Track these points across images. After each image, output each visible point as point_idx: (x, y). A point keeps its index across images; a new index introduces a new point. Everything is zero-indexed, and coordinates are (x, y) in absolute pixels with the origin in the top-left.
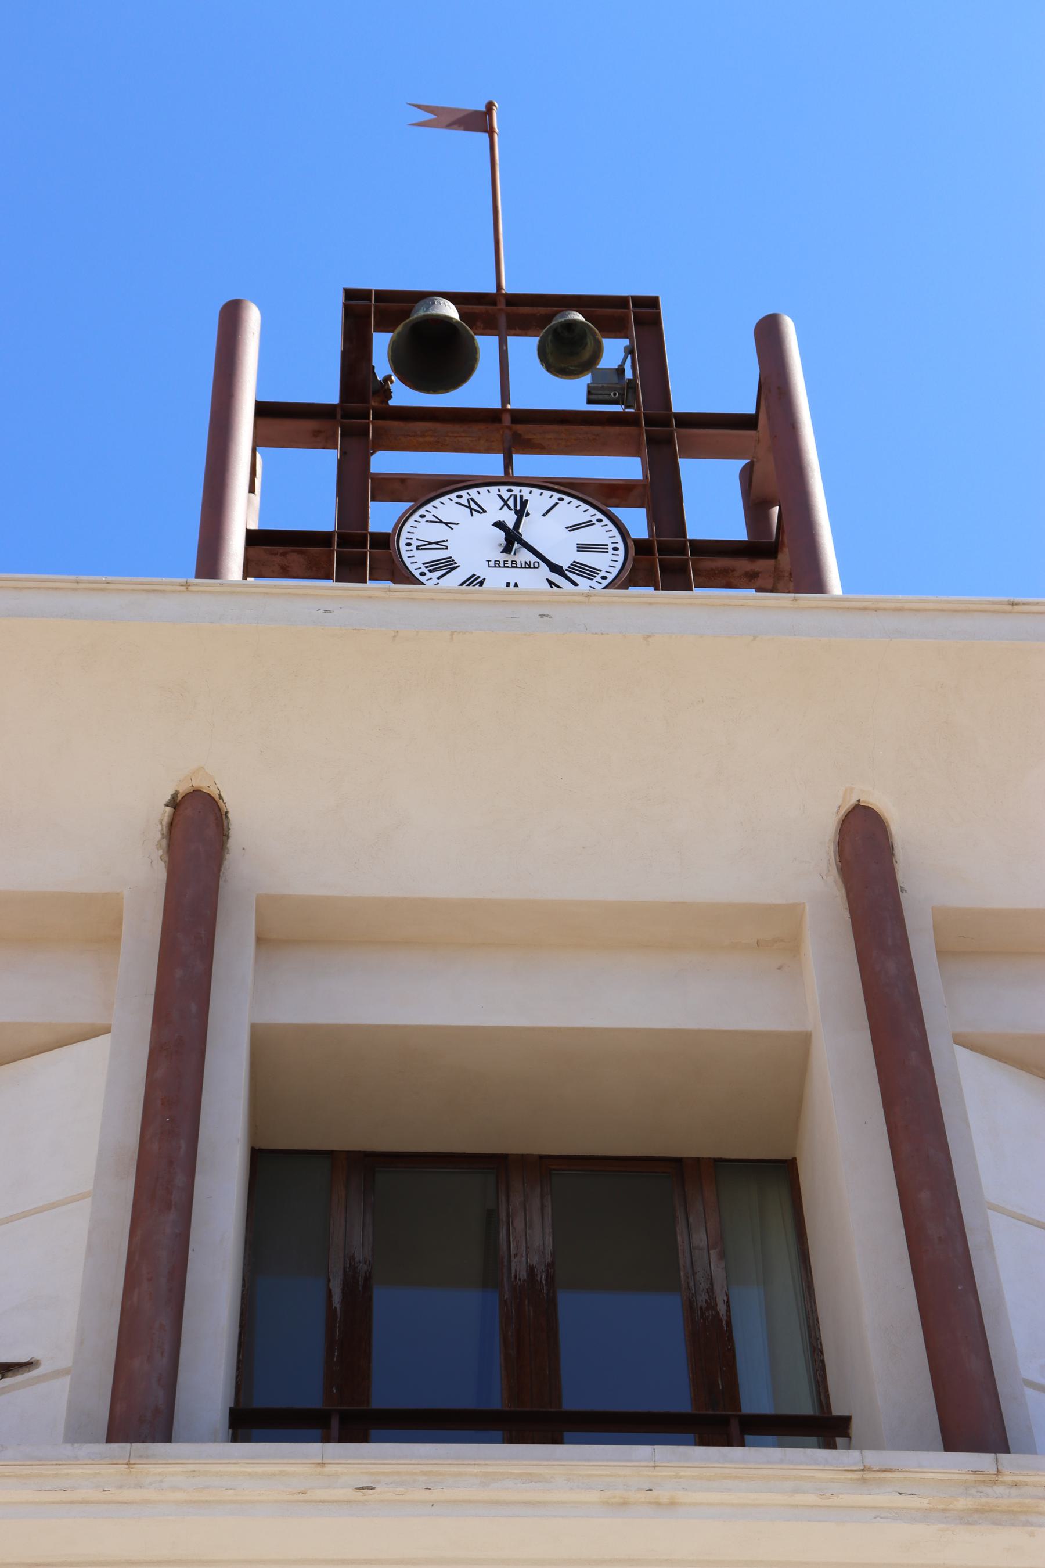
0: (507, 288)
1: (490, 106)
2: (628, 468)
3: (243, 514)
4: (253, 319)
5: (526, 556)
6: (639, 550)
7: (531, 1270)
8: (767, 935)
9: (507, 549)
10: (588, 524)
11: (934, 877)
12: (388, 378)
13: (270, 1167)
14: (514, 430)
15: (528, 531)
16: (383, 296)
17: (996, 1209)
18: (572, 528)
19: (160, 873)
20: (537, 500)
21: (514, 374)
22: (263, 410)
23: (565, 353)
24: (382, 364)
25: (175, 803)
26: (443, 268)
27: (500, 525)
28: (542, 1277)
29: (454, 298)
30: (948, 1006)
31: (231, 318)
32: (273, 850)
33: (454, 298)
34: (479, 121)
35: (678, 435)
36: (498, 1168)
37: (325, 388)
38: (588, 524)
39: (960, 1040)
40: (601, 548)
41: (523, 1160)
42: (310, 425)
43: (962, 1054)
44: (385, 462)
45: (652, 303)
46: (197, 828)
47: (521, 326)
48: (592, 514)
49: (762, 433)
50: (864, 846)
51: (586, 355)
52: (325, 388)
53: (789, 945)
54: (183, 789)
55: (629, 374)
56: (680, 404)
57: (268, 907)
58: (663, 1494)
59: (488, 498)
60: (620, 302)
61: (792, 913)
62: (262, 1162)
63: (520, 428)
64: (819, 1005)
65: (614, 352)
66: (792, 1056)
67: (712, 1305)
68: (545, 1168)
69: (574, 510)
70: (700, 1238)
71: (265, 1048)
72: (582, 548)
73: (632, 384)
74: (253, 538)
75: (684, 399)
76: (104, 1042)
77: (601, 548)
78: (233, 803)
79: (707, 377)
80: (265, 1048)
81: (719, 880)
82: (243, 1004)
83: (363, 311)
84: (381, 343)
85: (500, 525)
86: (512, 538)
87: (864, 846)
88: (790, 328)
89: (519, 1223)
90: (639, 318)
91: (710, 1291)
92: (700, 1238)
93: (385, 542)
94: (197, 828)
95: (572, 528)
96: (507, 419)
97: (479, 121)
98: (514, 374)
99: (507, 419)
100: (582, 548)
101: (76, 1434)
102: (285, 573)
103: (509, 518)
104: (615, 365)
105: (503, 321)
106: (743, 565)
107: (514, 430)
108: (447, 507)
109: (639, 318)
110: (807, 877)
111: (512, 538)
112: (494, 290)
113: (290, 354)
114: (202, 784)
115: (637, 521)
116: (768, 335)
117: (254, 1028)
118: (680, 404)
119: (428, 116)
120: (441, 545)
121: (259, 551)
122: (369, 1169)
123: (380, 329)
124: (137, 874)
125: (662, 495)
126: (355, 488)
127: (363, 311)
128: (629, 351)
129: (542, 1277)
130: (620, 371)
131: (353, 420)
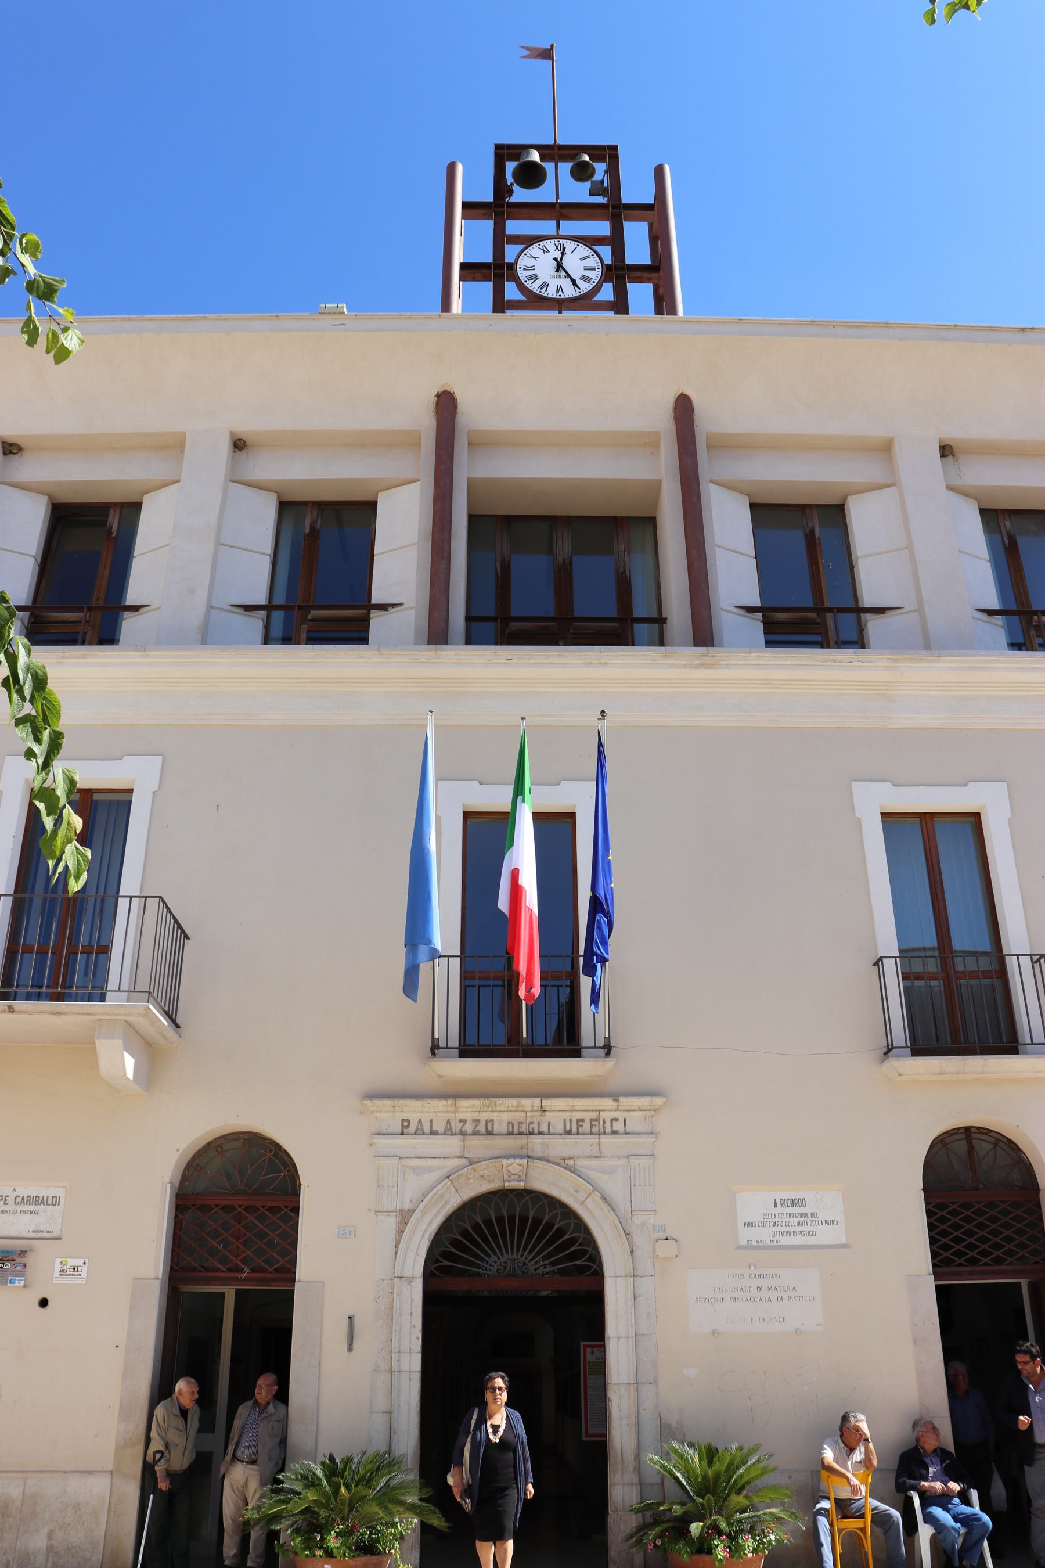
0: (560, 142)
1: (552, 46)
2: (602, 228)
3: (458, 257)
4: (460, 169)
5: (563, 273)
6: (607, 269)
7: (564, 560)
8: (648, 442)
9: (557, 271)
10: (588, 257)
11: (708, 421)
12: (512, 184)
13: (474, 520)
14: (560, 211)
15: (566, 263)
16: (510, 147)
17: (719, 547)
18: (582, 259)
19: (434, 422)
20: (569, 245)
21: (563, 185)
22: (466, 205)
23: (581, 172)
24: (509, 178)
25: (438, 396)
26: (531, 131)
27: (555, 259)
28: (568, 562)
29: (537, 147)
30: (707, 467)
31: (451, 169)
32: (475, 412)
33: (537, 147)
34: (547, 54)
35: (624, 212)
36: (553, 522)
37: (487, 195)
38: (588, 257)
39: (712, 482)
40: (592, 268)
41: (561, 517)
42: (482, 211)
43: (712, 486)
44: (513, 227)
45: (614, 148)
46: (446, 405)
47: (565, 158)
48: (589, 252)
49: (654, 211)
50: (683, 408)
51: (589, 172)
52: (487, 195)
53: (656, 445)
54: (441, 391)
55: (606, 185)
56: (625, 199)
57: (471, 433)
58: (603, 661)
59: (550, 244)
60: (602, 148)
61: (657, 434)
62: (472, 518)
63: (563, 211)
64: (662, 469)
65: (600, 169)
66: (654, 489)
67: (625, 572)
68: (569, 521)
69: (583, 250)
70: (622, 547)
71: (472, 484)
72: (586, 268)
73: (606, 189)
74: (463, 266)
75: (627, 197)
76: (417, 485)
77: (592, 268)
78: (458, 395)
79: (635, 189)
80: (472, 484)
81: (632, 423)
82: (466, 469)
83: (503, 153)
84: (510, 167)
85: (555, 259)
86: (559, 266)
87: (683, 408)
88: (667, 169)
89: (560, 542)
90: (609, 154)
91: (624, 567)
92: (622, 547)
93: (512, 267)
94: (446, 405)
95: (582, 259)
96: (558, 207)
97: (547, 54)
98: (563, 185)
99: (558, 207)
100: (586, 268)
101: (416, 643)
102: (474, 279)
103: (558, 255)
104: (600, 179)
105: (557, 157)
106: (647, 275)
107: (560, 211)
108: (535, 250)
109: (609, 154)
110: (663, 422)
111: (559, 266)
112: (552, 143)
113: (474, 182)
114: (448, 389)
115: (606, 252)
116: (659, 172)
117: (468, 479)
118: (625, 199)
119: (528, 53)
120: (532, 268)
121: (465, 272)
122: (508, 521)
123: (509, 160)
124: (426, 422)
125: (616, 241)
126: (500, 240)
127: (503, 153)
128: (606, 172)
129: (568, 562)
130: (602, 182)
131: (497, 209)
